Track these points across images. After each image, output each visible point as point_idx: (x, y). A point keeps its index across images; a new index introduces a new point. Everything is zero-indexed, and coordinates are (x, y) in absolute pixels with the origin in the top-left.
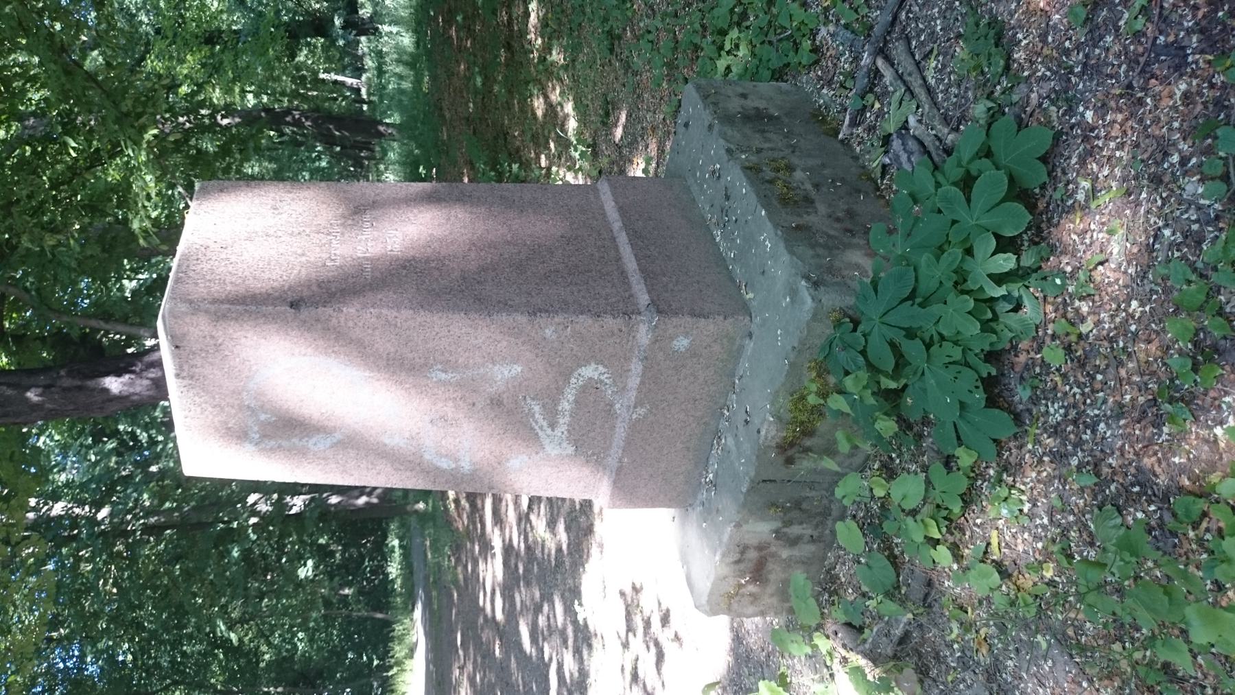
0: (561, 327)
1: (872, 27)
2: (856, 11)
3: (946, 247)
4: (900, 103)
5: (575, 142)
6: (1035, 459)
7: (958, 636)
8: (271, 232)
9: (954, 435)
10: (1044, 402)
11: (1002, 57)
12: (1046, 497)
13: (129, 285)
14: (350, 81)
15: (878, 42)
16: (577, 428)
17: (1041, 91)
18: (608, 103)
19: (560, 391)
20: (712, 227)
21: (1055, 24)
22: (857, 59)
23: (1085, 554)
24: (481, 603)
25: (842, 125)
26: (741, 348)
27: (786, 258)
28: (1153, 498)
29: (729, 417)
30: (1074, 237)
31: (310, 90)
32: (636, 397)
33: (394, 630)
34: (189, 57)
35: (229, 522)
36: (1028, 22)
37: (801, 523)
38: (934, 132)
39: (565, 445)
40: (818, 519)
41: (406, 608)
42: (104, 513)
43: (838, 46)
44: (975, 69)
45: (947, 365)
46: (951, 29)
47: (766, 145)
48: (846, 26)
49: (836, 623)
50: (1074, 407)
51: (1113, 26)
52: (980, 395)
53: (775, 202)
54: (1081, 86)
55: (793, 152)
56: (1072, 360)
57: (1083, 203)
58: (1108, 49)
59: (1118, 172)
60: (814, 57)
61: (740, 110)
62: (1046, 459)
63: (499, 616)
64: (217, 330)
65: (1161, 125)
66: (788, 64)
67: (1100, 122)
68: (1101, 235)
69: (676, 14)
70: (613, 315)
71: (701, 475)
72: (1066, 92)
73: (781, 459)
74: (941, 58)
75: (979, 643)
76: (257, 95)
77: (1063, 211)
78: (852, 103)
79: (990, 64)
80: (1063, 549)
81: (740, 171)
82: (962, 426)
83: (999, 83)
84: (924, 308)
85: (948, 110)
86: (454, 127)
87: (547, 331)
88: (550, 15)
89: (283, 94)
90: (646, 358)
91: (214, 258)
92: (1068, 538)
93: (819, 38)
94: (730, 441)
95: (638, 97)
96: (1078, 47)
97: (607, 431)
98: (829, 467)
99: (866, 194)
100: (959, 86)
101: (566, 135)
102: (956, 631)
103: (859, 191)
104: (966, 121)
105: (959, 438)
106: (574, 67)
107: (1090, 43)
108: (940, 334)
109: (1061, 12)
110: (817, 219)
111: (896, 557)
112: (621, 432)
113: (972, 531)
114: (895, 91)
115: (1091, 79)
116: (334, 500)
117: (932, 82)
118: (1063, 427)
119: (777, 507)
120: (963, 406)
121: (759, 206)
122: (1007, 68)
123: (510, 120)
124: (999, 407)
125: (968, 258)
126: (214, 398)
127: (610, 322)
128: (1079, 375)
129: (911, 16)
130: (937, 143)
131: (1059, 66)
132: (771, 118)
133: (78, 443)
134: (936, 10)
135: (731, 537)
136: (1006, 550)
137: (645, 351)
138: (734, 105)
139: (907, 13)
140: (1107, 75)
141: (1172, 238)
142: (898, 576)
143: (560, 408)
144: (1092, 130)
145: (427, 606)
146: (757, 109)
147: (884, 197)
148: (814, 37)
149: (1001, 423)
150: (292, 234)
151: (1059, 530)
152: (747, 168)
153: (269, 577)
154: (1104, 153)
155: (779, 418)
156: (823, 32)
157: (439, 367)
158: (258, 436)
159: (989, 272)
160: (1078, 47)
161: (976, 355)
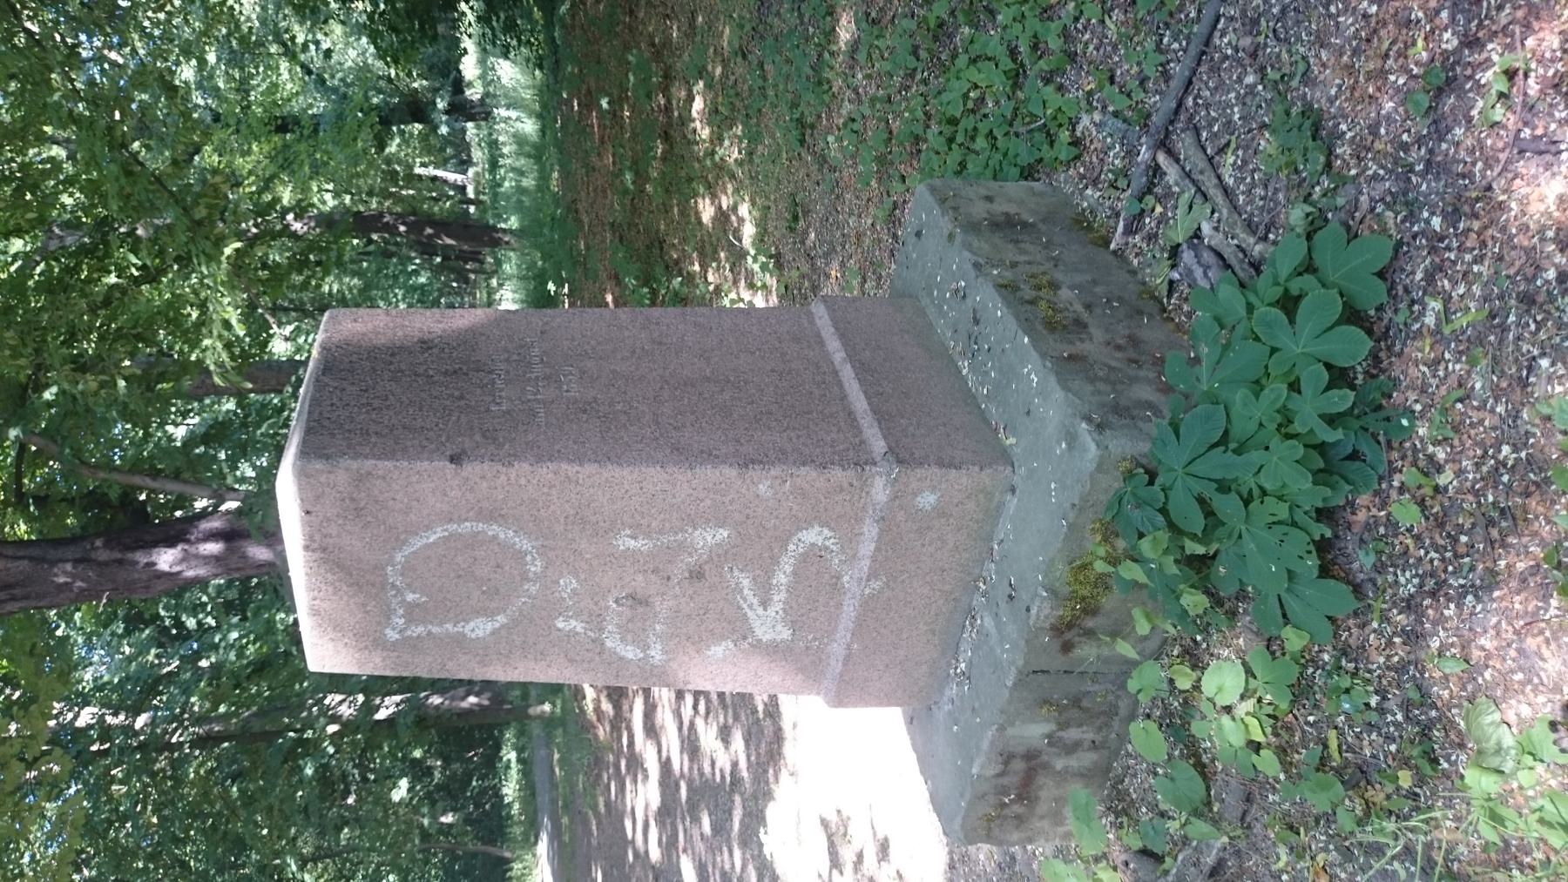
0: (780, 481)
1: (1149, 116)
2: (1129, 95)
3: (1264, 381)
4: (1191, 207)
5: (752, 252)
6: (1383, 641)
7: (1287, 864)
8: (421, 370)
9: (1279, 612)
10: (1391, 569)
11: (1321, 153)
12: (1399, 687)
13: (179, 433)
14: (452, 177)
15: (1159, 133)
16: (795, 606)
17: (1372, 193)
18: (796, 205)
19: (775, 561)
20: (956, 357)
21: (1388, 113)
22: (1131, 153)
23: (1453, 758)
25: (1113, 233)
26: (1001, 506)
27: (1058, 394)
28: (1541, 688)
30: (1424, 369)
31: (402, 188)
32: (870, 568)
33: (511, 869)
34: (255, 148)
35: (302, 731)
36: (1353, 110)
37: (1080, 725)
38: (1236, 242)
39: (779, 627)
40: (1103, 719)
41: (526, 840)
42: (141, 721)
43: (1104, 138)
44: (1287, 165)
45: (1270, 526)
46: (1253, 118)
47: (1022, 258)
48: (1116, 114)
49: (1126, 851)
50: (1431, 576)
51: (1464, 117)
52: (1312, 562)
53: (1040, 327)
54: (1424, 187)
55: (1056, 266)
56: (1427, 518)
57: (1432, 327)
58: (1458, 144)
59: (1476, 289)
60: (1074, 151)
61: (985, 215)
62: (1397, 640)
63: (655, 854)
65: (1530, 234)
66: (1041, 160)
67: (1451, 230)
68: (1458, 367)
69: (890, 98)
70: (843, 466)
71: (949, 665)
72: (1405, 194)
73: (1057, 645)
74: (1240, 153)
75: (1316, 873)
76: (337, 194)
77: (1407, 336)
78: (1125, 202)
79: (1306, 160)
80: (1425, 752)
81: (993, 290)
82: (1292, 604)
83: (1318, 183)
84: (1240, 455)
85: (1252, 214)
86: (594, 234)
87: (761, 486)
88: (720, 99)
89: (370, 194)
90: (883, 518)
91: (353, 403)
92: (1430, 739)
93: (1079, 129)
94: (989, 622)
95: (838, 197)
96: (1419, 141)
97: (832, 610)
98: (1123, 653)
99: (1151, 317)
100: (1266, 187)
101: (740, 241)
102: (1284, 858)
103: (1140, 313)
104: (1277, 229)
105: (1284, 616)
106: (751, 161)
107: (1435, 136)
108: (1261, 488)
109: (1396, 99)
110: (1094, 345)
111: (1204, 766)
112: (849, 610)
113: (1303, 732)
114: (1183, 192)
115: (1437, 179)
116: (436, 700)
117: (1231, 182)
118: (1419, 600)
119: (1051, 705)
120: (1291, 575)
121: (1020, 332)
122: (1329, 165)
123: (667, 225)
124: (1333, 577)
125: (1295, 395)
126: (351, 575)
127: (838, 475)
128: (1437, 537)
129: (1200, 102)
130: (1241, 255)
131: (1396, 163)
132: (1025, 225)
133: (109, 631)
134: (1232, 95)
135: (992, 743)
136: (1348, 755)
137: (881, 510)
138: (979, 210)
139: (1195, 99)
140: (1458, 175)
141: (1552, 370)
142: (1208, 789)
143: (775, 582)
144: (1441, 240)
145: (555, 837)
146: (1007, 214)
147: (1173, 320)
148: (1074, 127)
149: (1337, 596)
150: (446, 373)
151: (1417, 729)
152: (1002, 286)
154: (1458, 268)
155: (1053, 592)
156: (1085, 120)
157: (628, 532)
158: (403, 620)
159: (1320, 412)
160: (1419, 141)
161: (1306, 513)
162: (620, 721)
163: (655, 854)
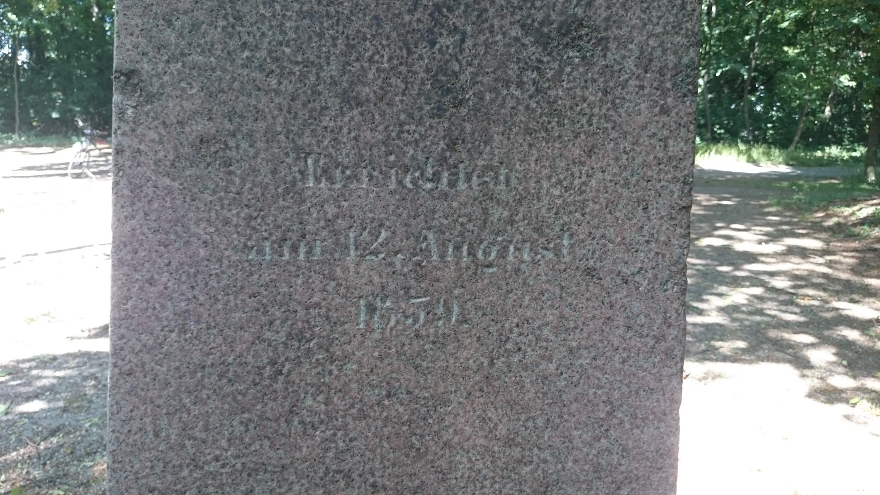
24: (733, 226)
145: (782, 177)
153: (733, 107)
162: (816, 229)
163: (705, 242)
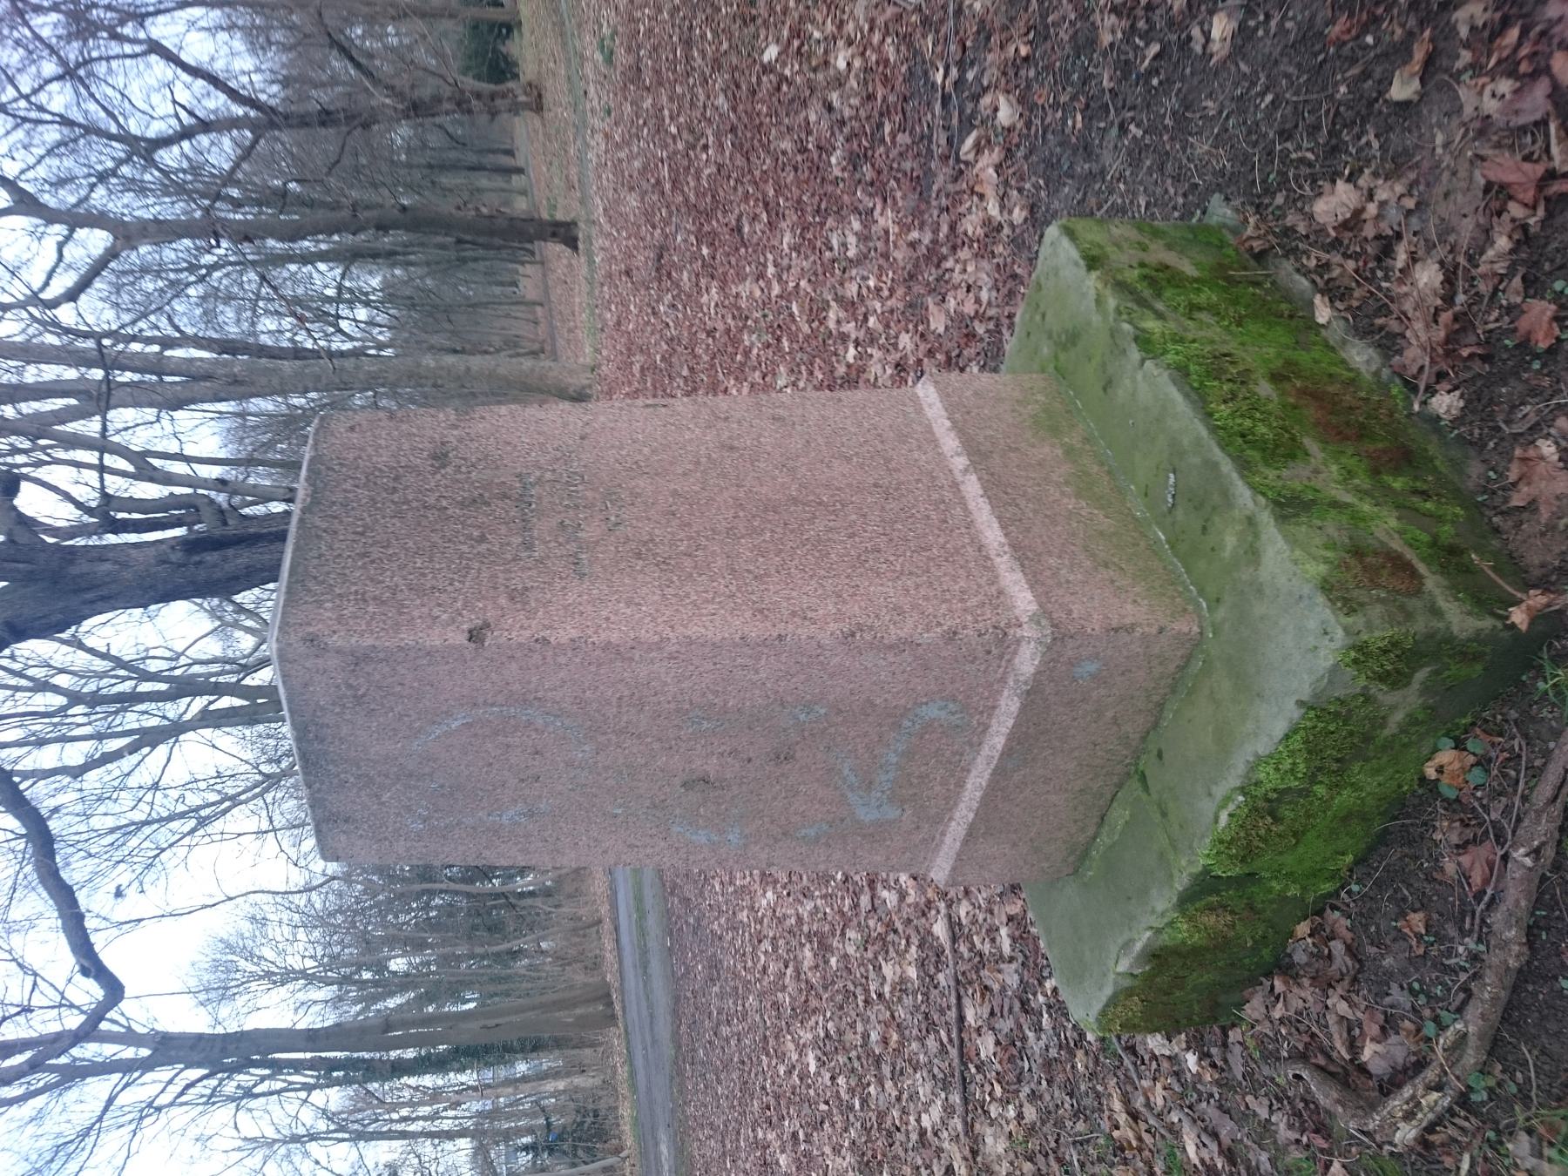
29: (1198, 198)
64: (357, 678)
